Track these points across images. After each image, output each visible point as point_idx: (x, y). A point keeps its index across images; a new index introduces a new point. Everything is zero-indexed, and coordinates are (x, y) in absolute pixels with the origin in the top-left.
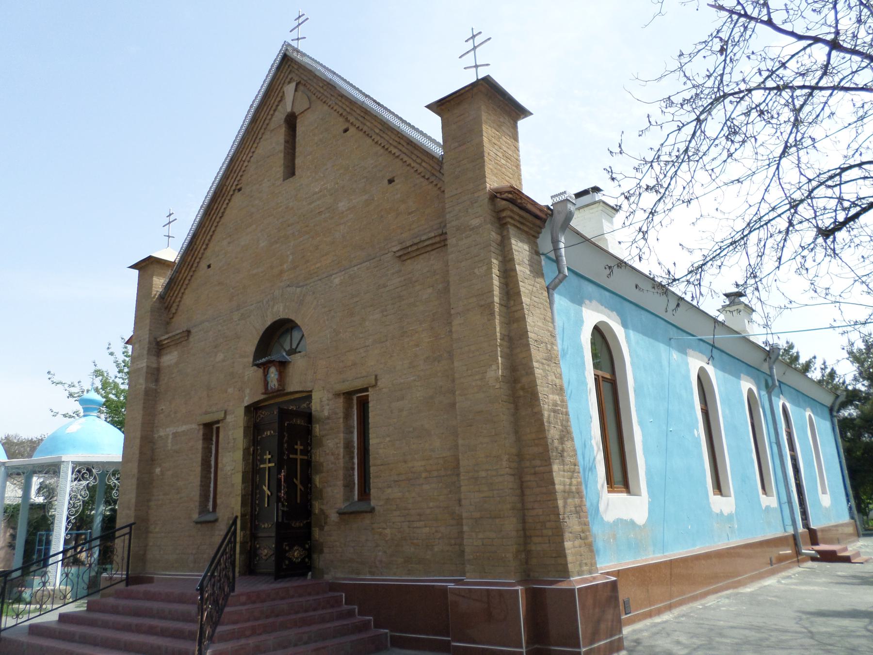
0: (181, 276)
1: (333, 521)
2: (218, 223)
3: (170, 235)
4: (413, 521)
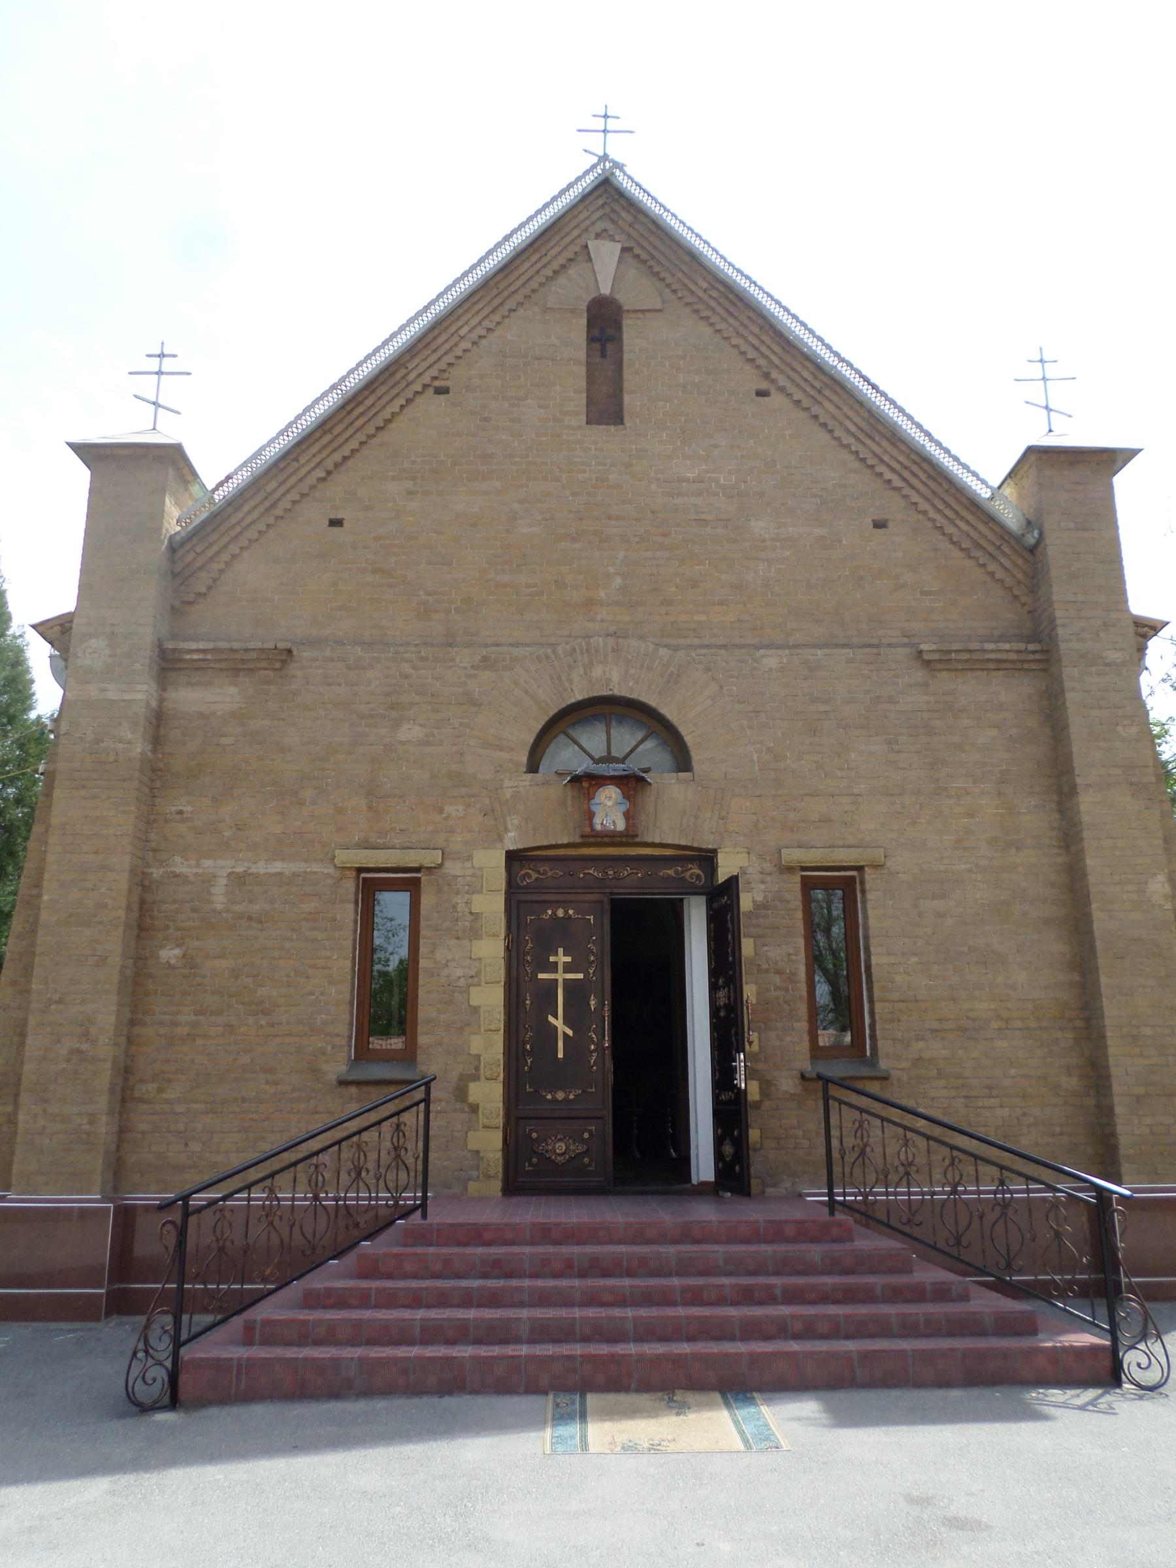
0: (240, 515)
1: (786, 1092)
2: (370, 437)
3: (161, 402)
4: (975, 1097)
